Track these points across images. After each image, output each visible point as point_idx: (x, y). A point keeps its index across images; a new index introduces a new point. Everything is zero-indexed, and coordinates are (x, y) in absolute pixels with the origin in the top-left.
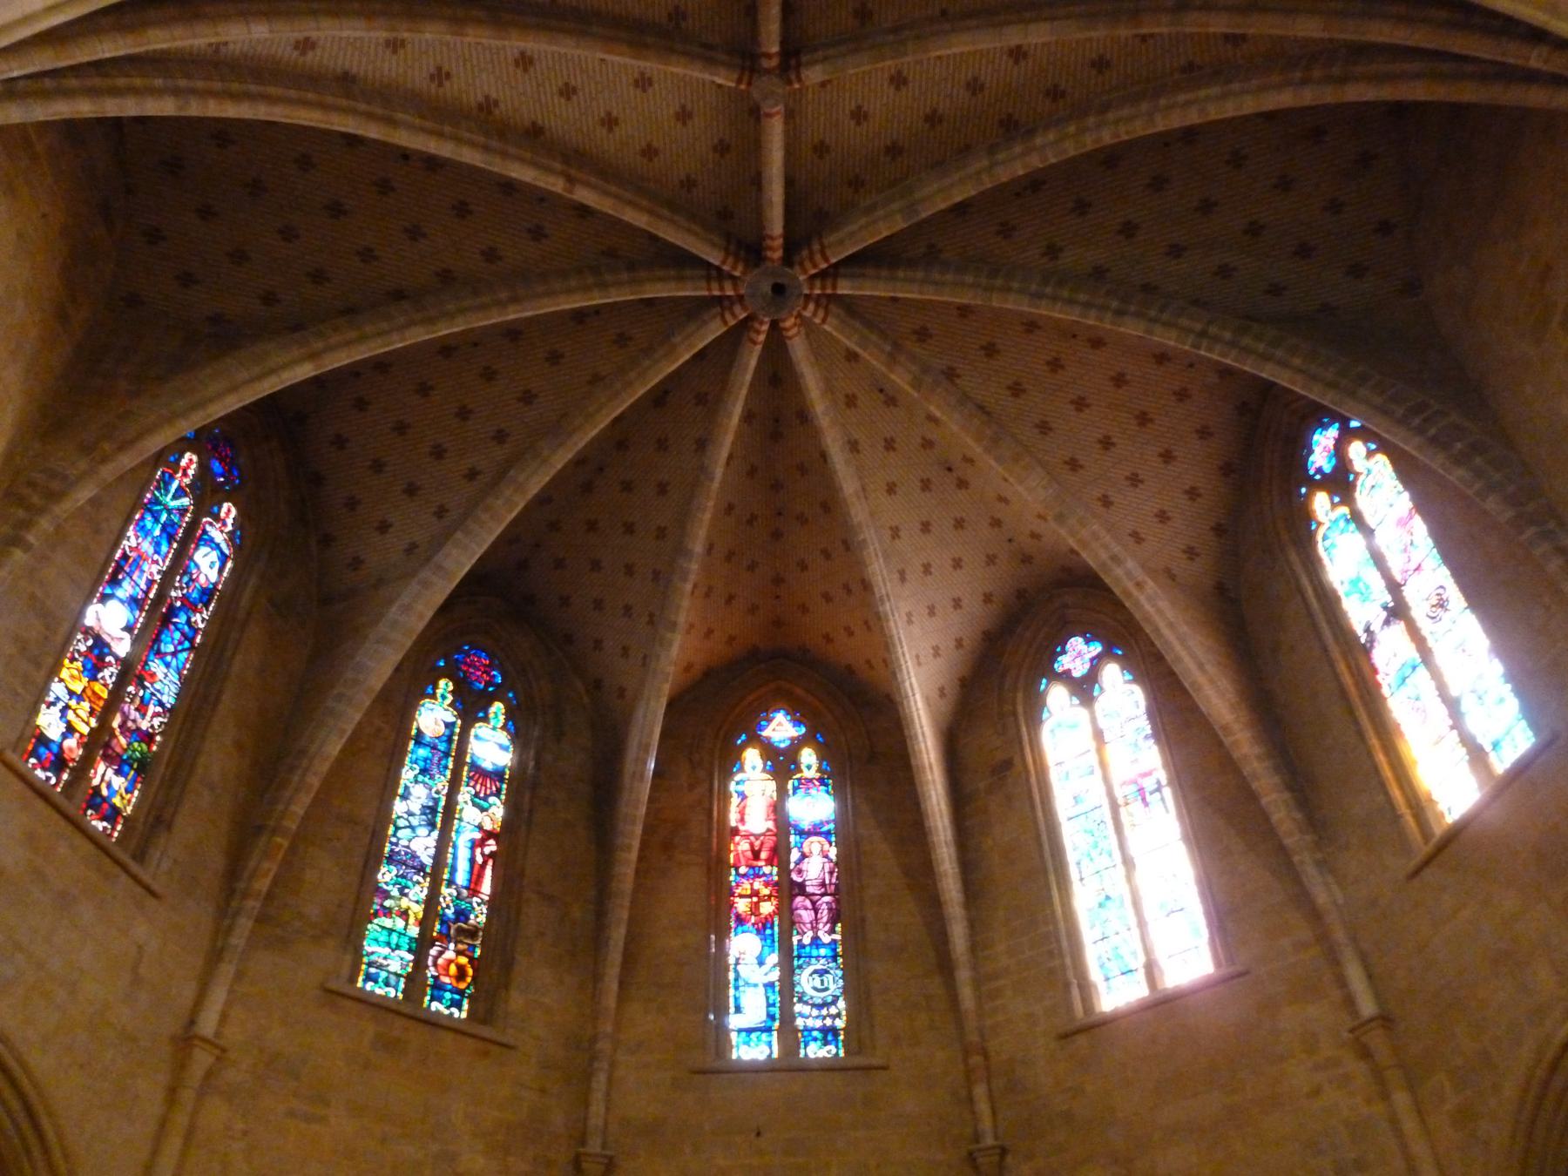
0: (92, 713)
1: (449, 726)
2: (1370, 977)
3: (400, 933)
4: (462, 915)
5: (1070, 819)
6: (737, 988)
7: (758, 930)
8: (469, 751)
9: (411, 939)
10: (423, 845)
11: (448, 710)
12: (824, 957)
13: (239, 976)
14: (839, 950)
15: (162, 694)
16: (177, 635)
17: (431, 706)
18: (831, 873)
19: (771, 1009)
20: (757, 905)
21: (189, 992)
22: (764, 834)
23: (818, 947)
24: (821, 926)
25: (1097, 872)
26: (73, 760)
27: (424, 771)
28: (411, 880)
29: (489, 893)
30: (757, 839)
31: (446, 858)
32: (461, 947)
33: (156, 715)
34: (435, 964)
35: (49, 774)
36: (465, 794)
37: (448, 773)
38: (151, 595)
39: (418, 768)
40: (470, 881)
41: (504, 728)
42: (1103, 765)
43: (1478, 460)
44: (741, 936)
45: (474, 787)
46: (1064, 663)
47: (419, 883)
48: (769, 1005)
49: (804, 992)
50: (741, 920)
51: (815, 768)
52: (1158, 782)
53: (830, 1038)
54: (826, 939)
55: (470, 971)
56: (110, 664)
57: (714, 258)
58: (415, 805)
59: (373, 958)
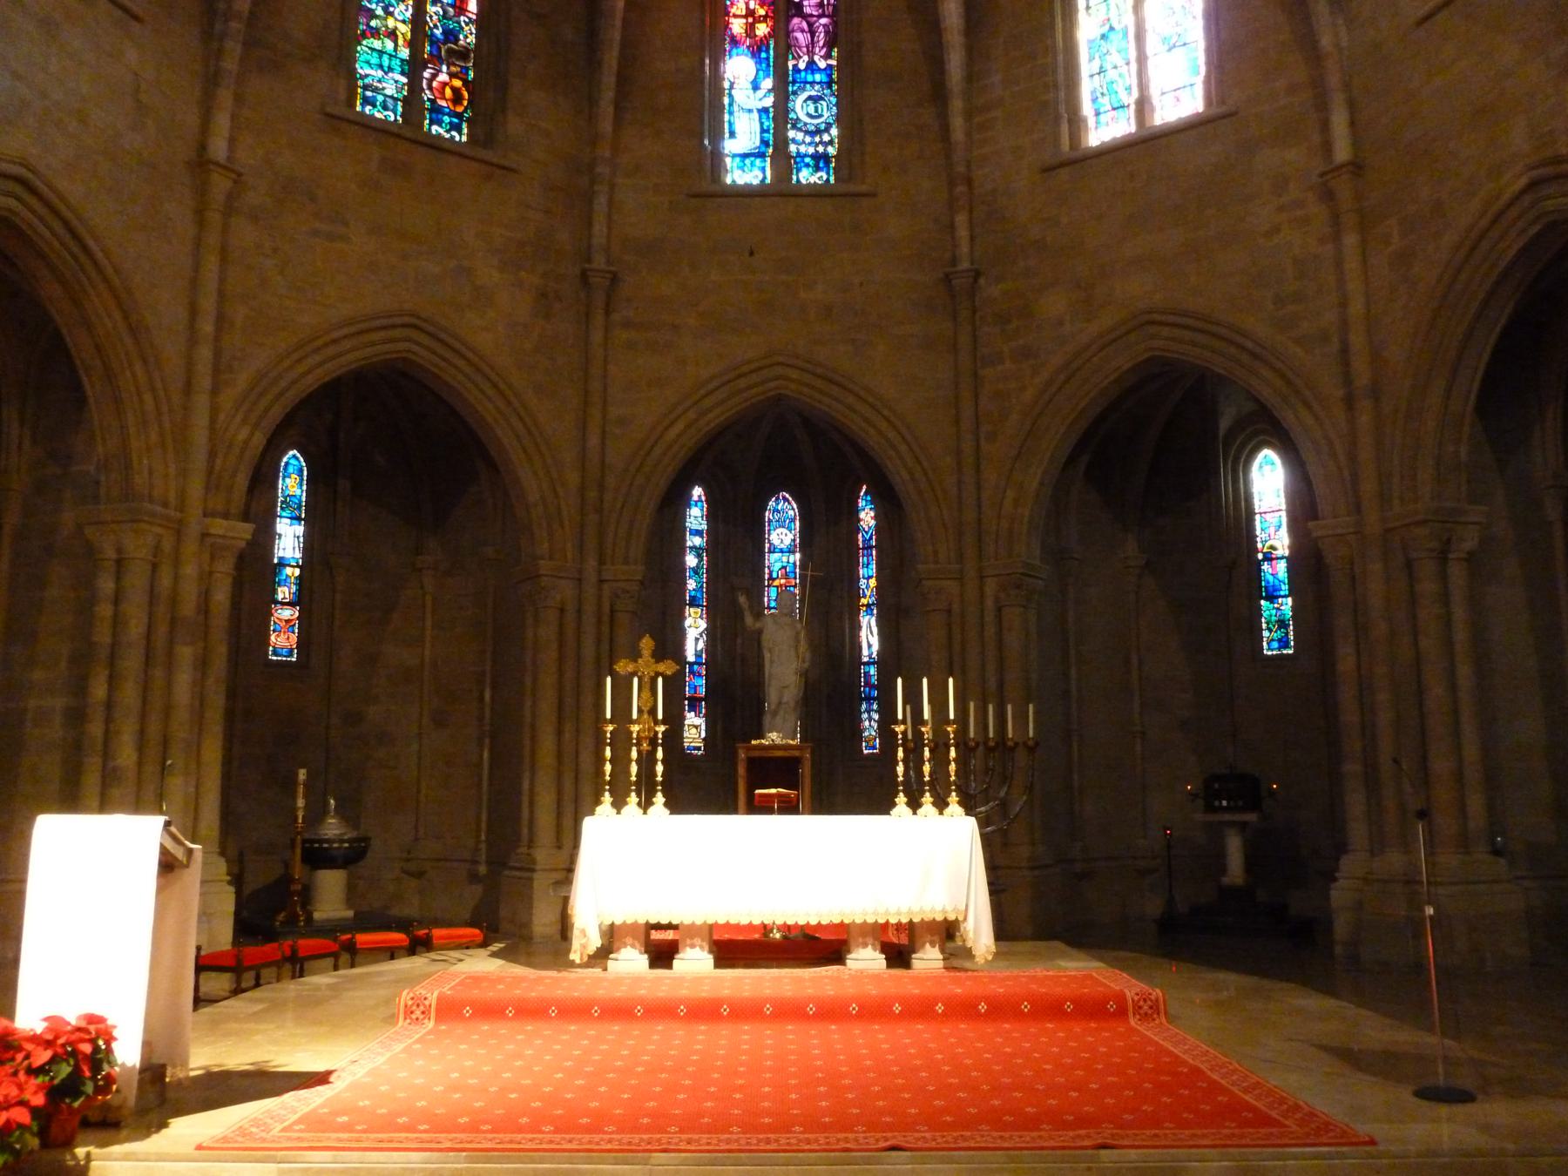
3: (391, 55)
4: (451, 36)
6: (731, 113)
9: (402, 60)
12: (818, 83)
13: (239, 99)
14: (834, 76)
19: (766, 135)
24: (817, 49)
29: (475, 11)
32: (453, 69)
34: (430, 88)
48: (763, 131)
49: (798, 119)
50: (735, 42)
53: (821, 165)
54: (822, 64)
55: (466, 95)
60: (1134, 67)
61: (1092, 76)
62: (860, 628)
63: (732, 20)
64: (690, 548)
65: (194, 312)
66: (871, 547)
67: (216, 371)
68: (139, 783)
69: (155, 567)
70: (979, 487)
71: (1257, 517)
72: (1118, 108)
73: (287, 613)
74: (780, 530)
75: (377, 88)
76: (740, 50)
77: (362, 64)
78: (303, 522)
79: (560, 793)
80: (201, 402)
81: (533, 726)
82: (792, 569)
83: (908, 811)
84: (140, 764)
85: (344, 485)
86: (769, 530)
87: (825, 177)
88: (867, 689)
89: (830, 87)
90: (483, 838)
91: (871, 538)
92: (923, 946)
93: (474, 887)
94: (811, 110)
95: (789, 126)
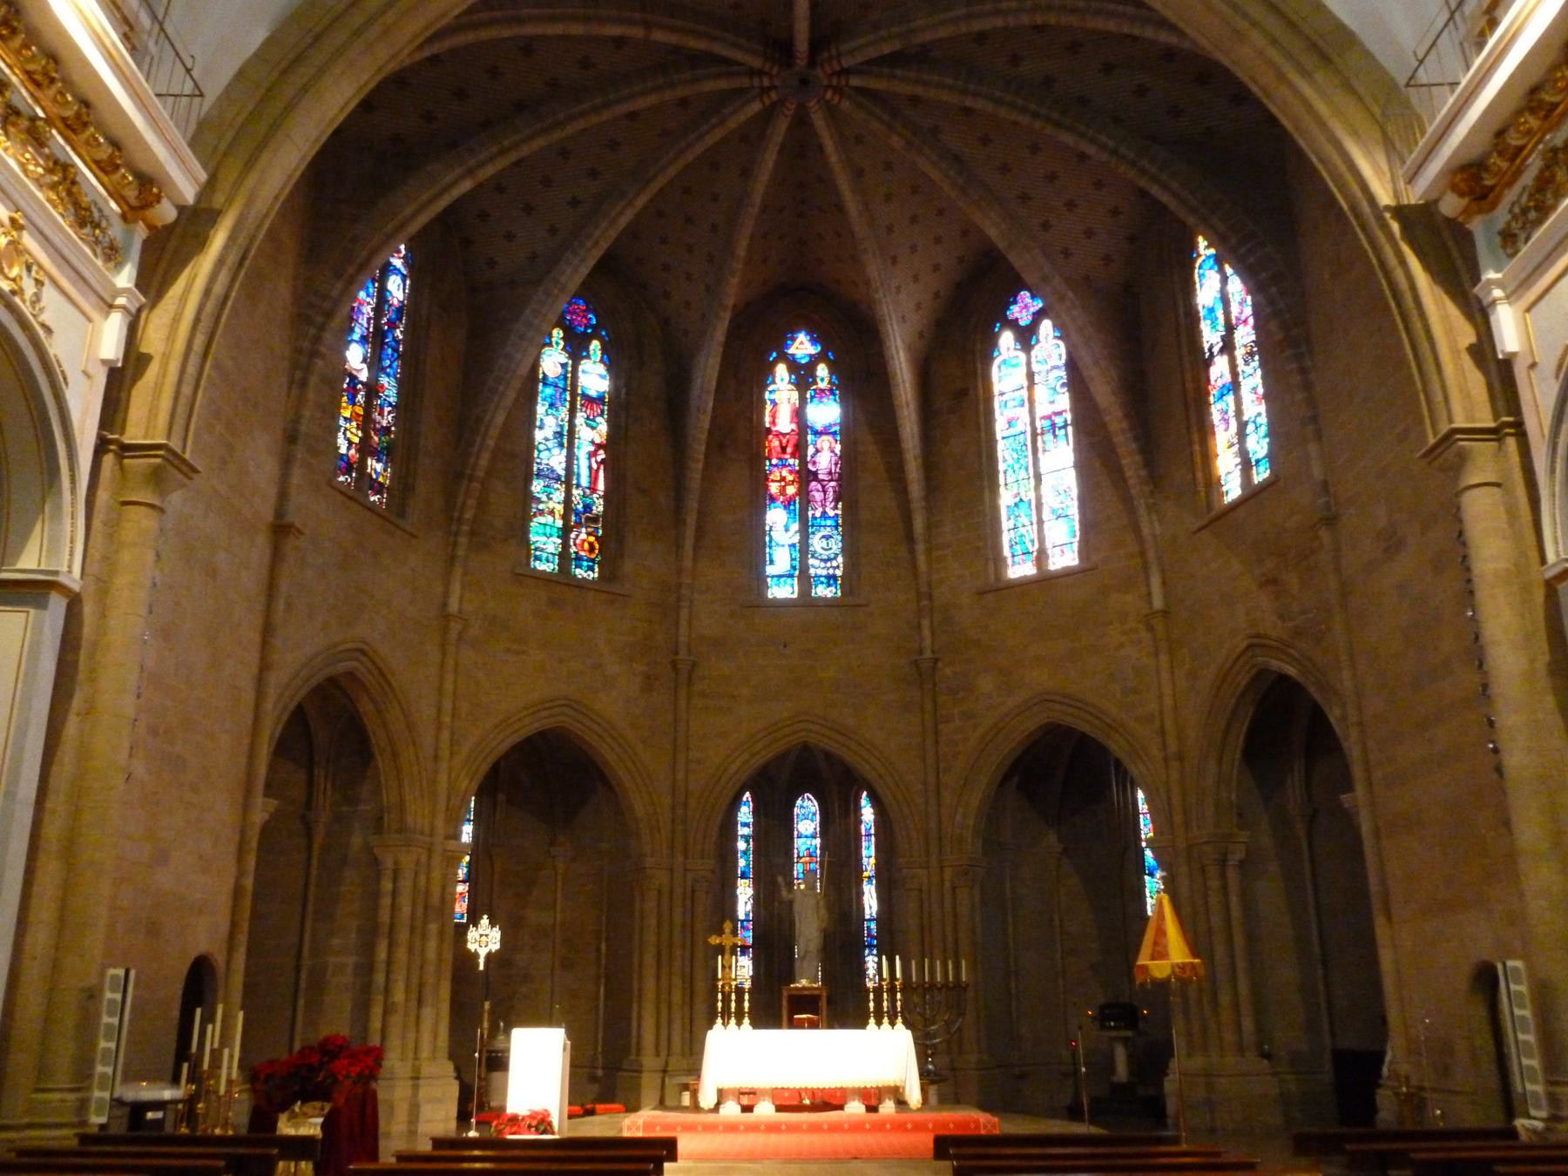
0: (358, 428)
1: (564, 366)
2: (1164, 583)
4: (588, 508)
5: (1004, 438)
6: (770, 547)
7: (785, 507)
13: (465, 574)
16: (390, 351)
17: (549, 353)
18: (836, 464)
20: (784, 487)
23: (826, 519)
24: (828, 504)
27: (552, 405)
32: (589, 530)
33: (389, 413)
36: (580, 418)
37: (567, 404)
38: (371, 330)
39: (547, 404)
40: (590, 482)
41: (602, 361)
43: (1274, 289)
44: (773, 511)
46: (1015, 311)
48: (792, 559)
50: (773, 499)
51: (826, 380)
52: (1066, 421)
53: (832, 582)
54: (831, 513)
55: (597, 546)
56: (360, 390)
57: (756, 63)
59: (538, 545)
60: (1035, 526)
62: (863, 894)
63: (771, 484)
65: (439, 710)
71: (1141, 816)
73: (461, 888)
76: (776, 504)
79: (658, 1013)
80: (444, 765)
81: (640, 972)
84: (407, 1000)
85: (501, 797)
87: (834, 590)
89: (837, 529)
90: (600, 1050)
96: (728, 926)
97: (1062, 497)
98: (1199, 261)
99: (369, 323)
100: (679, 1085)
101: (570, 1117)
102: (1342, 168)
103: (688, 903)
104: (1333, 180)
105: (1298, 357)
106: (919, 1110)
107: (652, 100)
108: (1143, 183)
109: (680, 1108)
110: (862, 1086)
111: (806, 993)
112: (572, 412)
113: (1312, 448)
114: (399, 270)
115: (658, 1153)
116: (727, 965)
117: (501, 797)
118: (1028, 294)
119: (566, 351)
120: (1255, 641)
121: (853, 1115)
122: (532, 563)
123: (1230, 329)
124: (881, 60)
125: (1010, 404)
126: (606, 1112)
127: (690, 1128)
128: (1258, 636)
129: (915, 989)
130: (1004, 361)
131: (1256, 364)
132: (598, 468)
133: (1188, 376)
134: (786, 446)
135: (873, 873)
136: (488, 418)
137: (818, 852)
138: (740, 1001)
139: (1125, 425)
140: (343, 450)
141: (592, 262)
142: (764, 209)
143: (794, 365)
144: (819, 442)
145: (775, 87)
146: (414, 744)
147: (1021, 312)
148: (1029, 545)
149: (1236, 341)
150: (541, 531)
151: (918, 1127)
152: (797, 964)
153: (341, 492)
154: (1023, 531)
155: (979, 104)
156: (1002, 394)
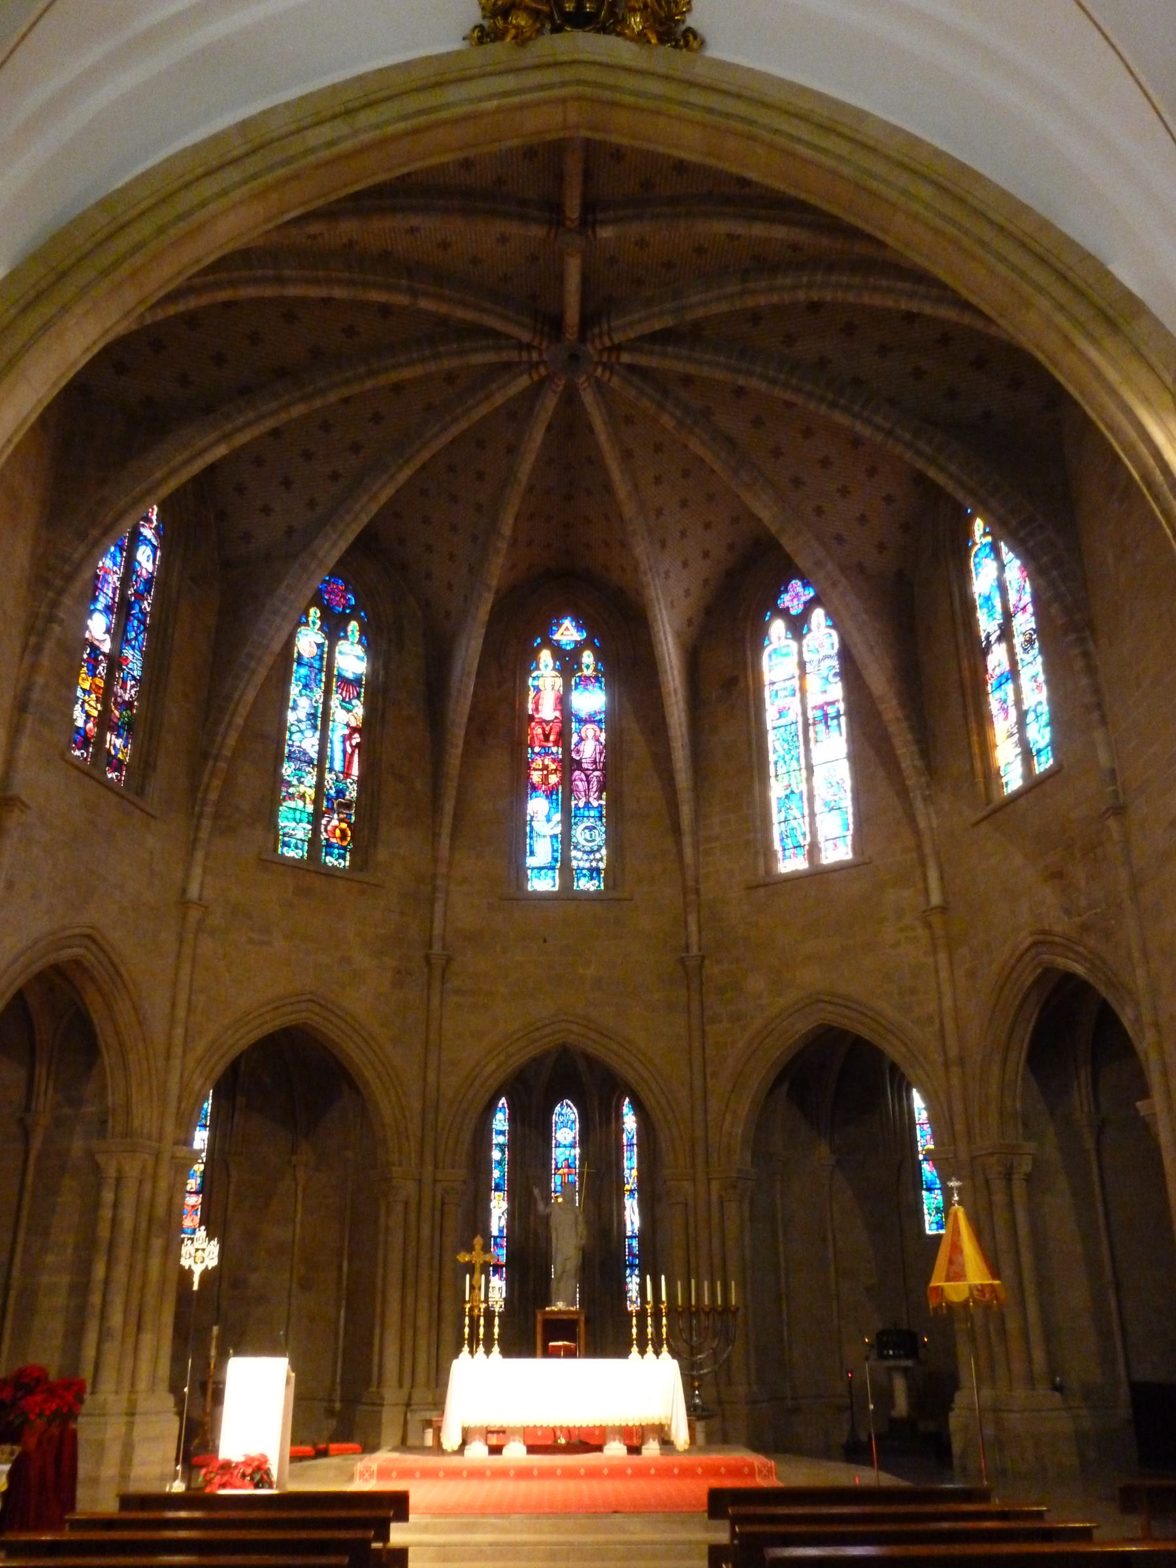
0: (97, 701)
1: (320, 646)
2: (942, 878)
3: (301, 811)
4: (340, 793)
5: (774, 728)
6: (531, 838)
8: (336, 665)
9: (309, 814)
10: (309, 743)
11: (317, 633)
12: (592, 817)
13: (207, 856)
14: (604, 812)
15: (133, 671)
16: (136, 623)
18: (601, 753)
19: (555, 854)
20: (547, 776)
21: (179, 875)
22: (552, 721)
24: (592, 794)
25: (788, 772)
26: (93, 737)
27: (306, 686)
28: (305, 771)
29: (357, 774)
30: (547, 725)
31: (327, 752)
33: (133, 687)
34: (326, 831)
35: (83, 751)
37: (322, 685)
38: (117, 600)
39: (301, 685)
40: (344, 766)
42: (803, 690)
43: (1055, 573)
45: (341, 694)
46: (785, 600)
47: (310, 773)
48: (554, 851)
49: (578, 842)
50: (535, 788)
51: (592, 667)
52: (838, 711)
53: (594, 875)
54: (595, 804)
55: (349, 833)
57: (526, 337)
58: (302, 713)
59: (286, 830)
60: (807, 819)
61: (780, 823)
63: (532, 772)
64: (496, 1144)
65: (174, 1005)
66: (633, 1145)
67: (185, 1043)
68: (287, 1340)
69: (141, 1182)
70: (706, 1112)
71: (918, 1127)
72: (797, 847)
73: (193, 1200)
74: (564, 1130)
75: (292, 835)
76: (538, 794)
77: (283, 819)
78: (208, 1129)
80: (176, 1063)
81: (383, 1292)
82: (573, 1160)
83: (654, 1356)
86: (556, 1130)
88: (631, 1258)
89: (601, 820)
91: (633, 1137)
92: (649, 1439)
93: (330, 1421)
94: (588, 837)
95: (572, 847)
96: (478, 1241)
97: (835, 789)
98: (975, 549)
99: (114, 594)
100: (422, 1421)
101: (296, 1458)
102: (1133, 435)
103: (438, 1215)
104: (1124, 449)
105: (1082, 641)
106: (686, 1451)
107: (418, 370)
108: (920, 464)
109: (421, 1449)
110: (624, 1424)
111: (565, 1317)
112: (327, 693)
113: (1098, 735)
114: (150, 541)
115: (380, 1513)
116: (477, 1286)
117: (241, 1100)
118: (800, 583)
119: (323, 631)
120: (1041, 937)
121: (612, 1457)
122: (280, 849)
123: (1008, 616)
124: (654, 337)
125: (781, 694)
126: (341, 1453)
127: (429, 1474)
128: (1044, 932)
129: (680, 1314)
130: (775, 650)
131: (1035, 651)
132: (353, 752)
133: (965, 664)
134: (550, 734)
135: (634, 1186)
136: (236, 696)
137: (577, 1163)
138: (489, 1325)
139: (900, 714)
140: (80, 723)
141: (350, 537)
142: (531, 489)
143: (558, 652)
144: (583, 730)
145: (545, 363)
146: (144, 1040)
147: (792, 601)
148: (801, 838)
149: (1014, 629)
150: (291, 816)
151: (687, 1472)
152: (554, 1285)
153: (77, 768)
154: (793, 823)
155: (755, 383)
156: (773, 683)
